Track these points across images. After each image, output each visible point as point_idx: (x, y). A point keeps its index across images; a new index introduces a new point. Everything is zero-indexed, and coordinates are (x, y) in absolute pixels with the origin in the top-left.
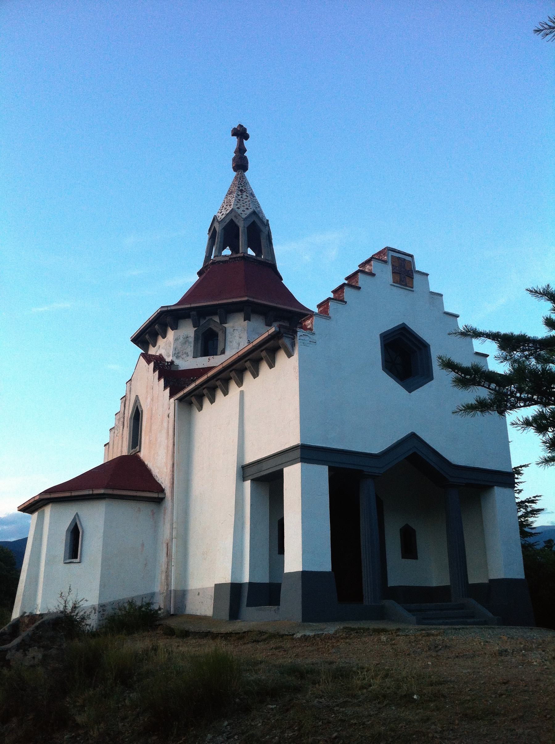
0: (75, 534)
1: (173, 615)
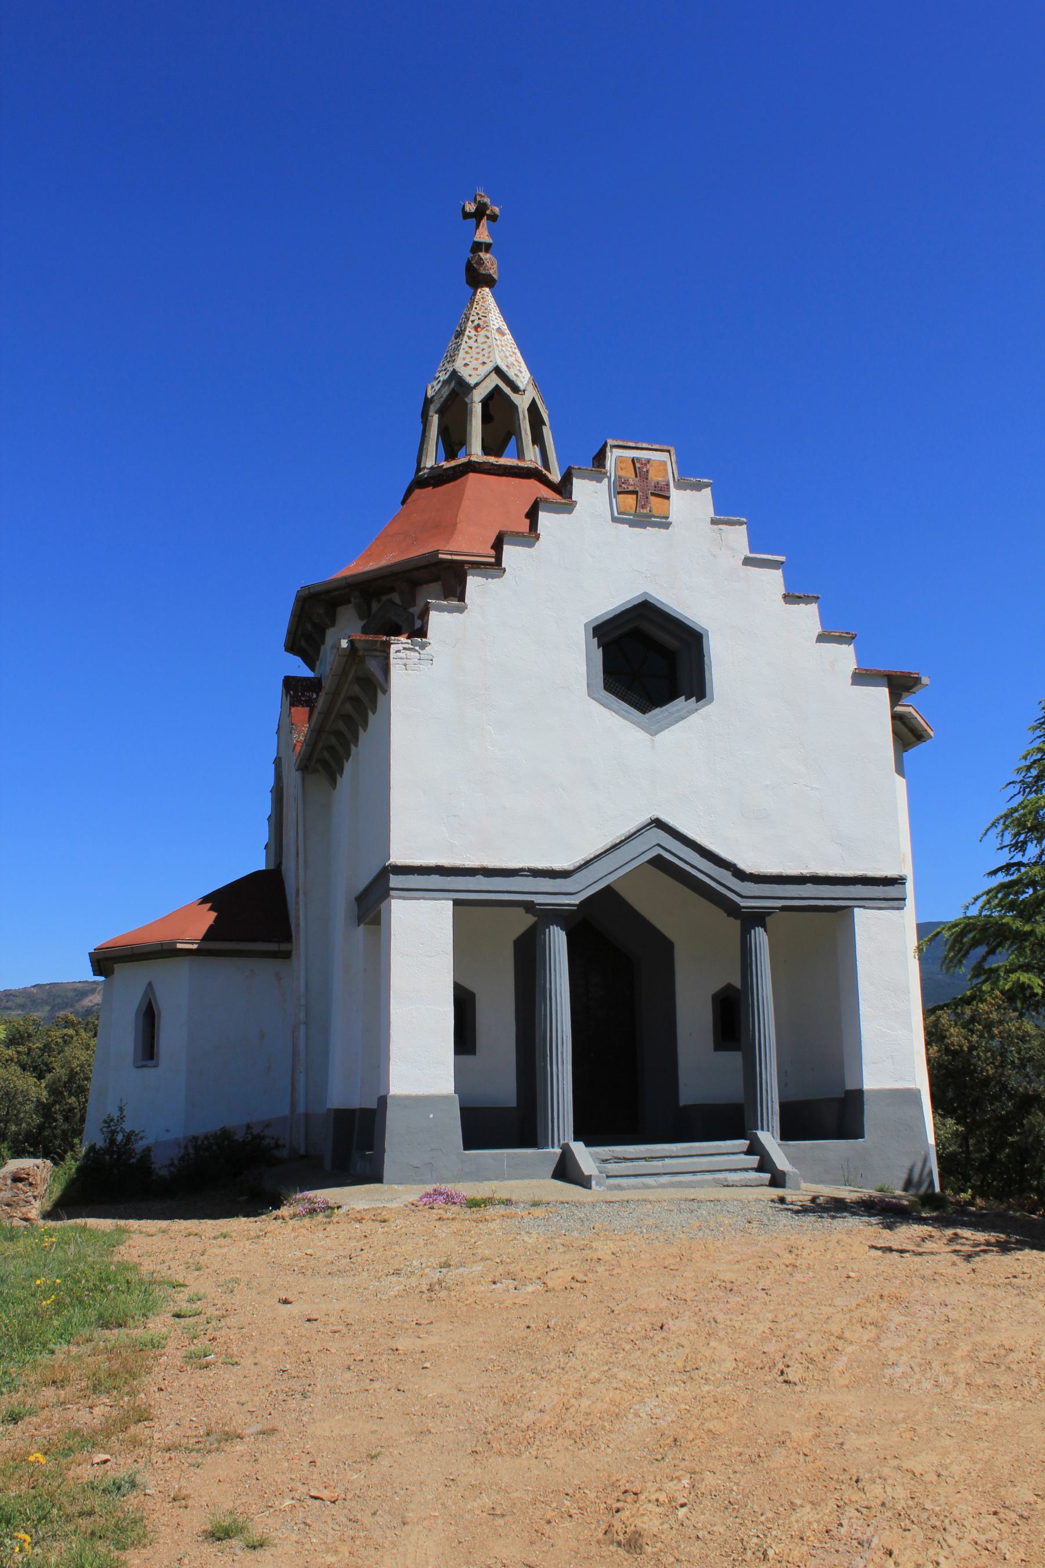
0: (149, 1017)
1: (303, 1157)
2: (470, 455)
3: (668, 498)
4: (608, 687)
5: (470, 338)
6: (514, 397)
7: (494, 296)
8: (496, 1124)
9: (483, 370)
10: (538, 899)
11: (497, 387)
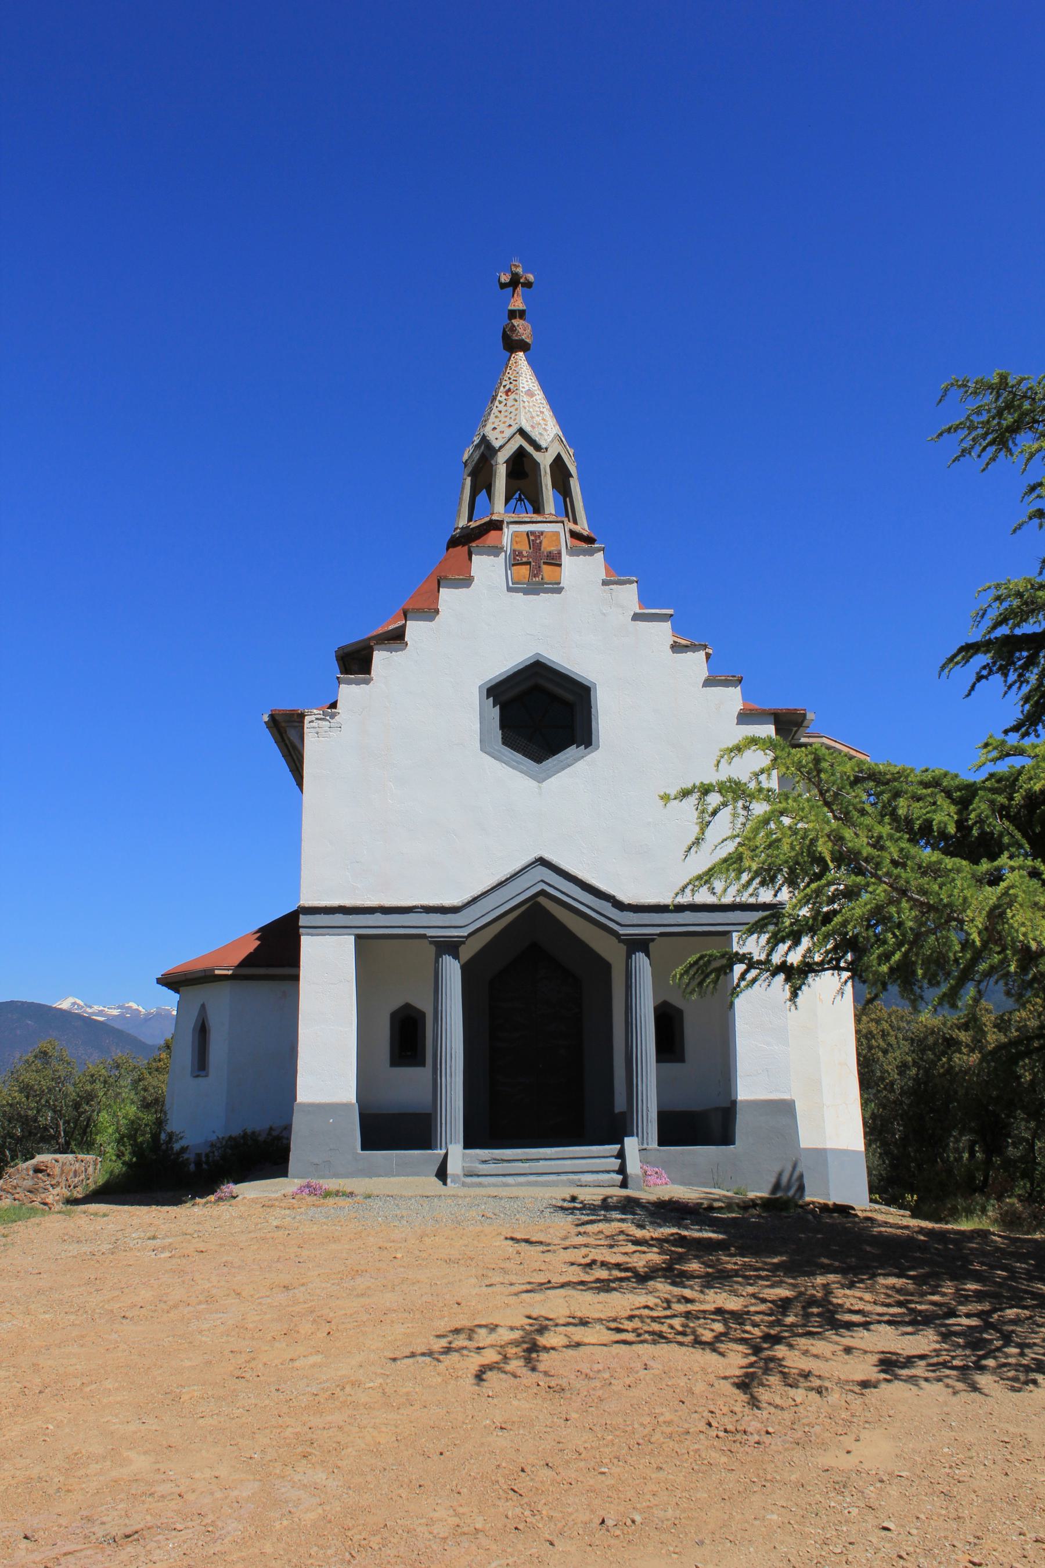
2: (492, 514)
3: (560, 565)
4: (507, 741)
5: (500, 402)
6: (536, 455)
7: (528, 360)
8: (391, 1128)
9: (509, 432)
10: (430, 932)
11: (521, 447)
